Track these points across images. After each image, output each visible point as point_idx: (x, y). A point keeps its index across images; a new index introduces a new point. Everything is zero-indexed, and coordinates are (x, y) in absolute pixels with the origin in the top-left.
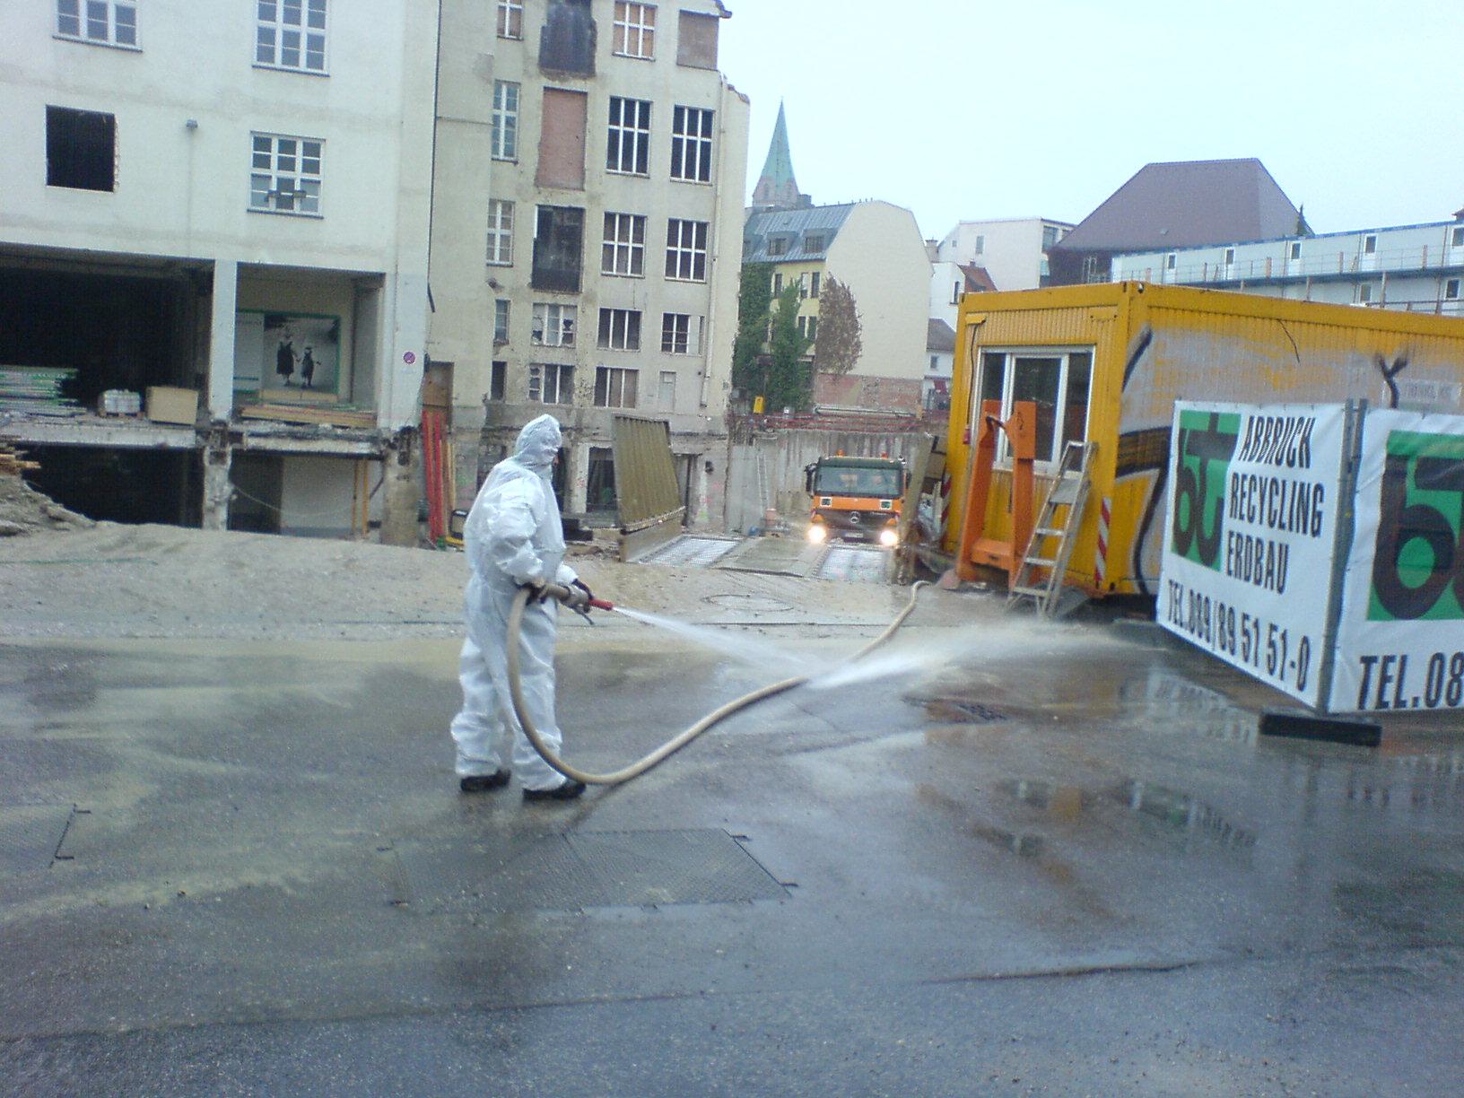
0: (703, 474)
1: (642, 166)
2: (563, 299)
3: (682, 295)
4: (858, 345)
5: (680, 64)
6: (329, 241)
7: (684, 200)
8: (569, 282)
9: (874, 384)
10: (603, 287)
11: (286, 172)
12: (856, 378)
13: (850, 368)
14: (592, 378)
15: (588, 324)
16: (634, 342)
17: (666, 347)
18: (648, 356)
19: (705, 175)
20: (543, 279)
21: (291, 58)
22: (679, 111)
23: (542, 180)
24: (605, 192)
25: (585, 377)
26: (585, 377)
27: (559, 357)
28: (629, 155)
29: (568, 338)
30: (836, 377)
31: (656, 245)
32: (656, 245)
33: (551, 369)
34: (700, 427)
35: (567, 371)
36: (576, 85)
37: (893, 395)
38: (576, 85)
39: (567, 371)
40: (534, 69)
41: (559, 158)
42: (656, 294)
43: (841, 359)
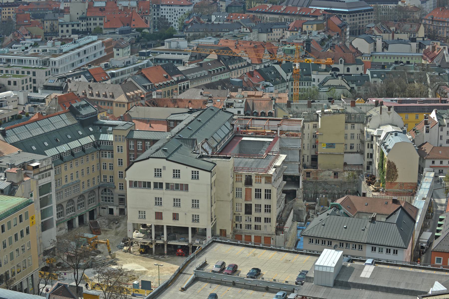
0: (272, 240)
1: (260, 198)
2: (249, 216)
3: (267, 215)
4: (397, 175)
5: (265, 183)
6: (200, 226)
7: (267, 202)
8: (250, 213)
9: (402, 184)
10: (255, 214)
11: (196, 219)
12: (397, 183)
13: (395, 180)
14: (254, 226)
15: (253, 219)
16: (260, 221)
17: (265, 222)
18: (262, 223)
19: (270, 198)
20: (246, 213)
21: (195, 207)
22: (266, 190)
23: (246, 200)
24: (254, 202)
25: (253, 226)
26: (253, 226)
27: (249, 223)
28: (258, 196)
29: (251, 221)
30: (391, 183)
31: (263, 208)
32: (263, 208)
33: (248, 225)
34: (271, 233)
35: (251, 225)
36: (250, 187)
37: (408, 186)
38: (250, 187)
39: (251, 225)
40: (244, 186)
41: (248, 197)
42: (263, 215)
43: (393, 179)
